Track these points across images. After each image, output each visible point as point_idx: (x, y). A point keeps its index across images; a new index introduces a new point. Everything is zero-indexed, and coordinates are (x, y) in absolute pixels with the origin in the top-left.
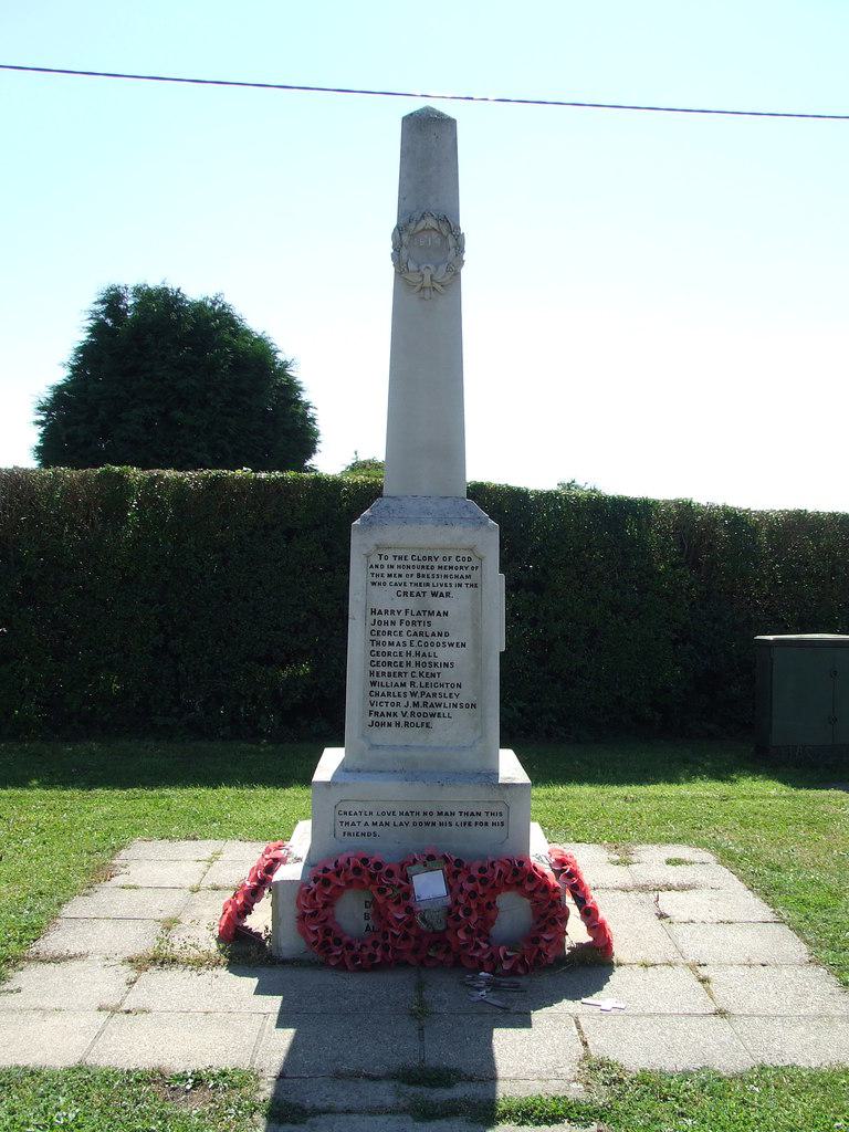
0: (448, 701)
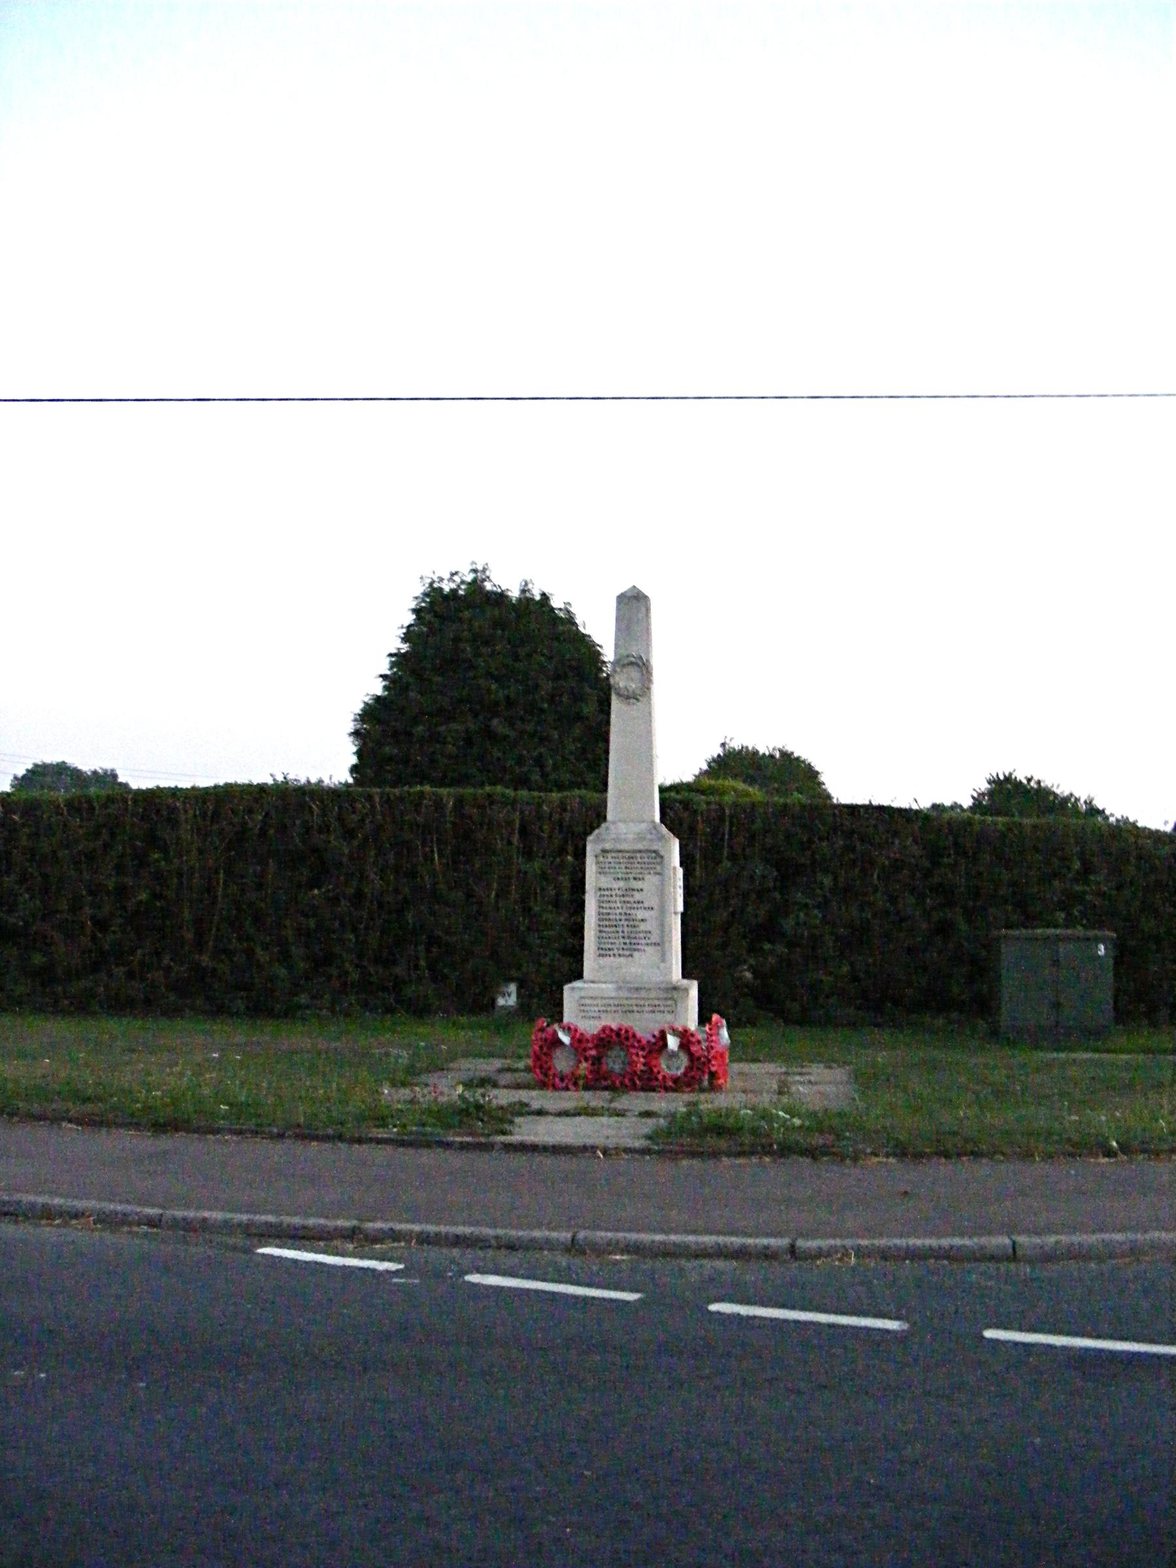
0: (643, 941)
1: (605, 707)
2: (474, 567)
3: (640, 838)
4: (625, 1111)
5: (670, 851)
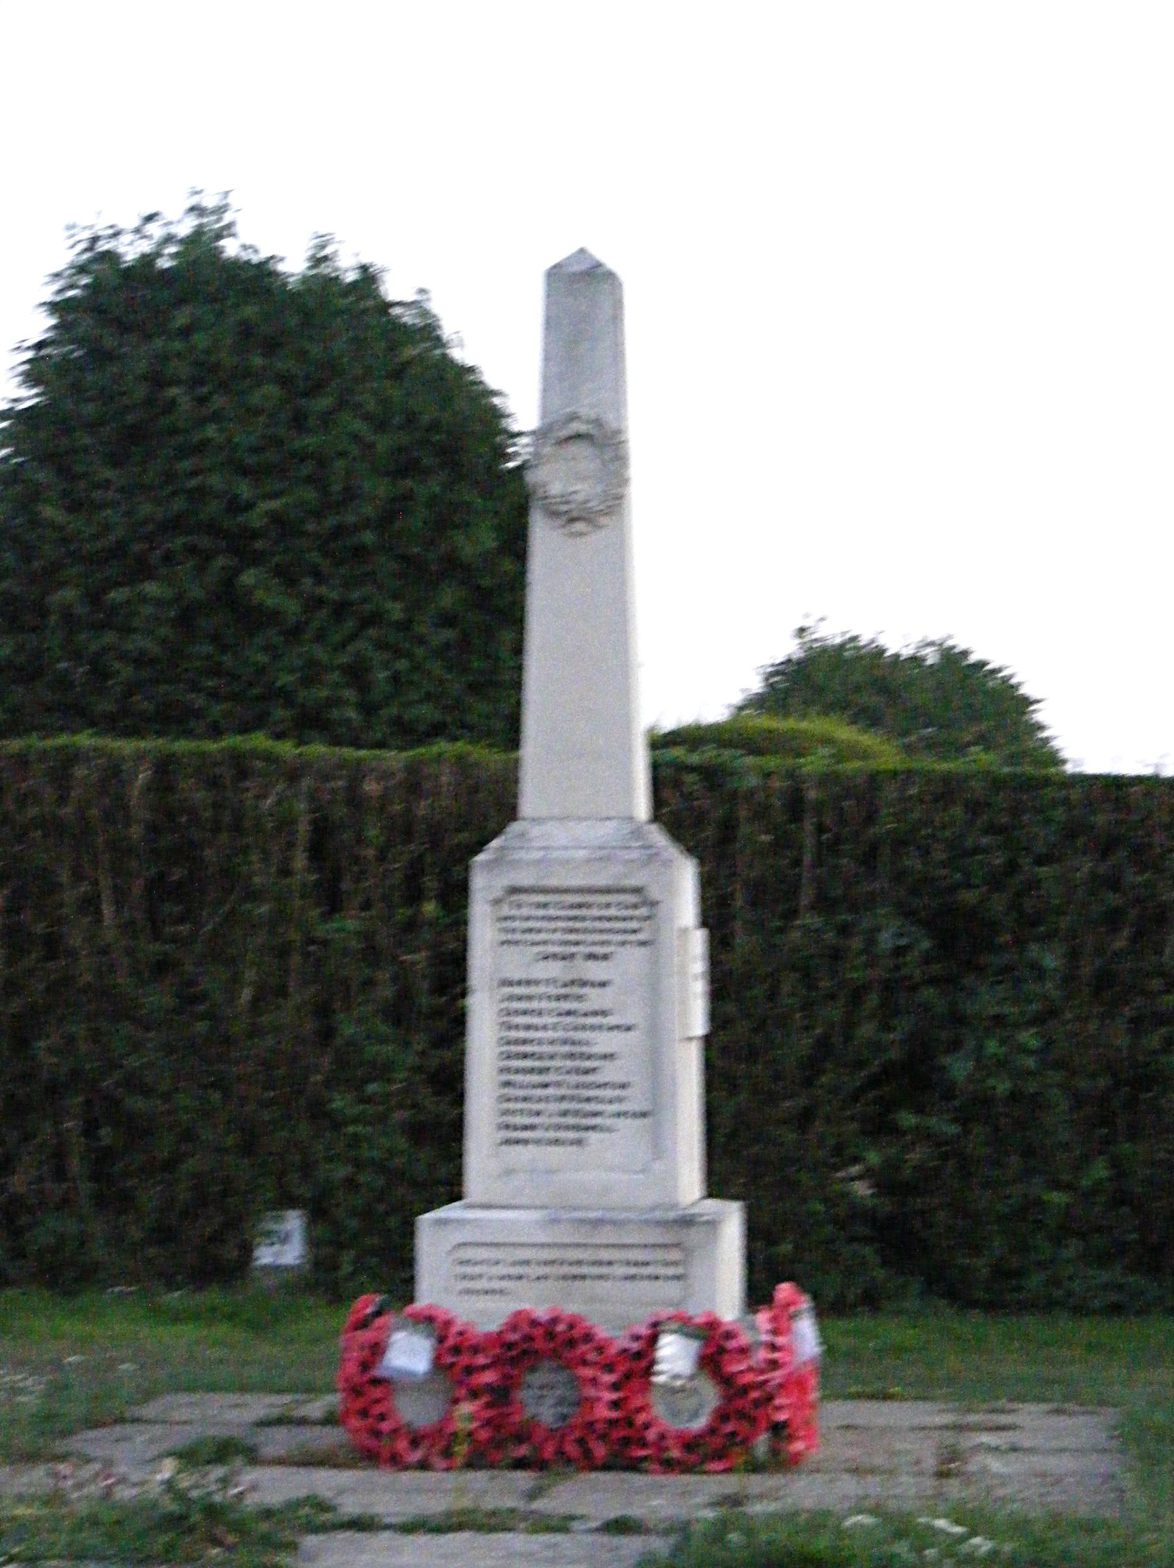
1: (516, 544)
2: (194, 201)
3: (603, 856)
4: (572, 1518)
5: (671, 888)
